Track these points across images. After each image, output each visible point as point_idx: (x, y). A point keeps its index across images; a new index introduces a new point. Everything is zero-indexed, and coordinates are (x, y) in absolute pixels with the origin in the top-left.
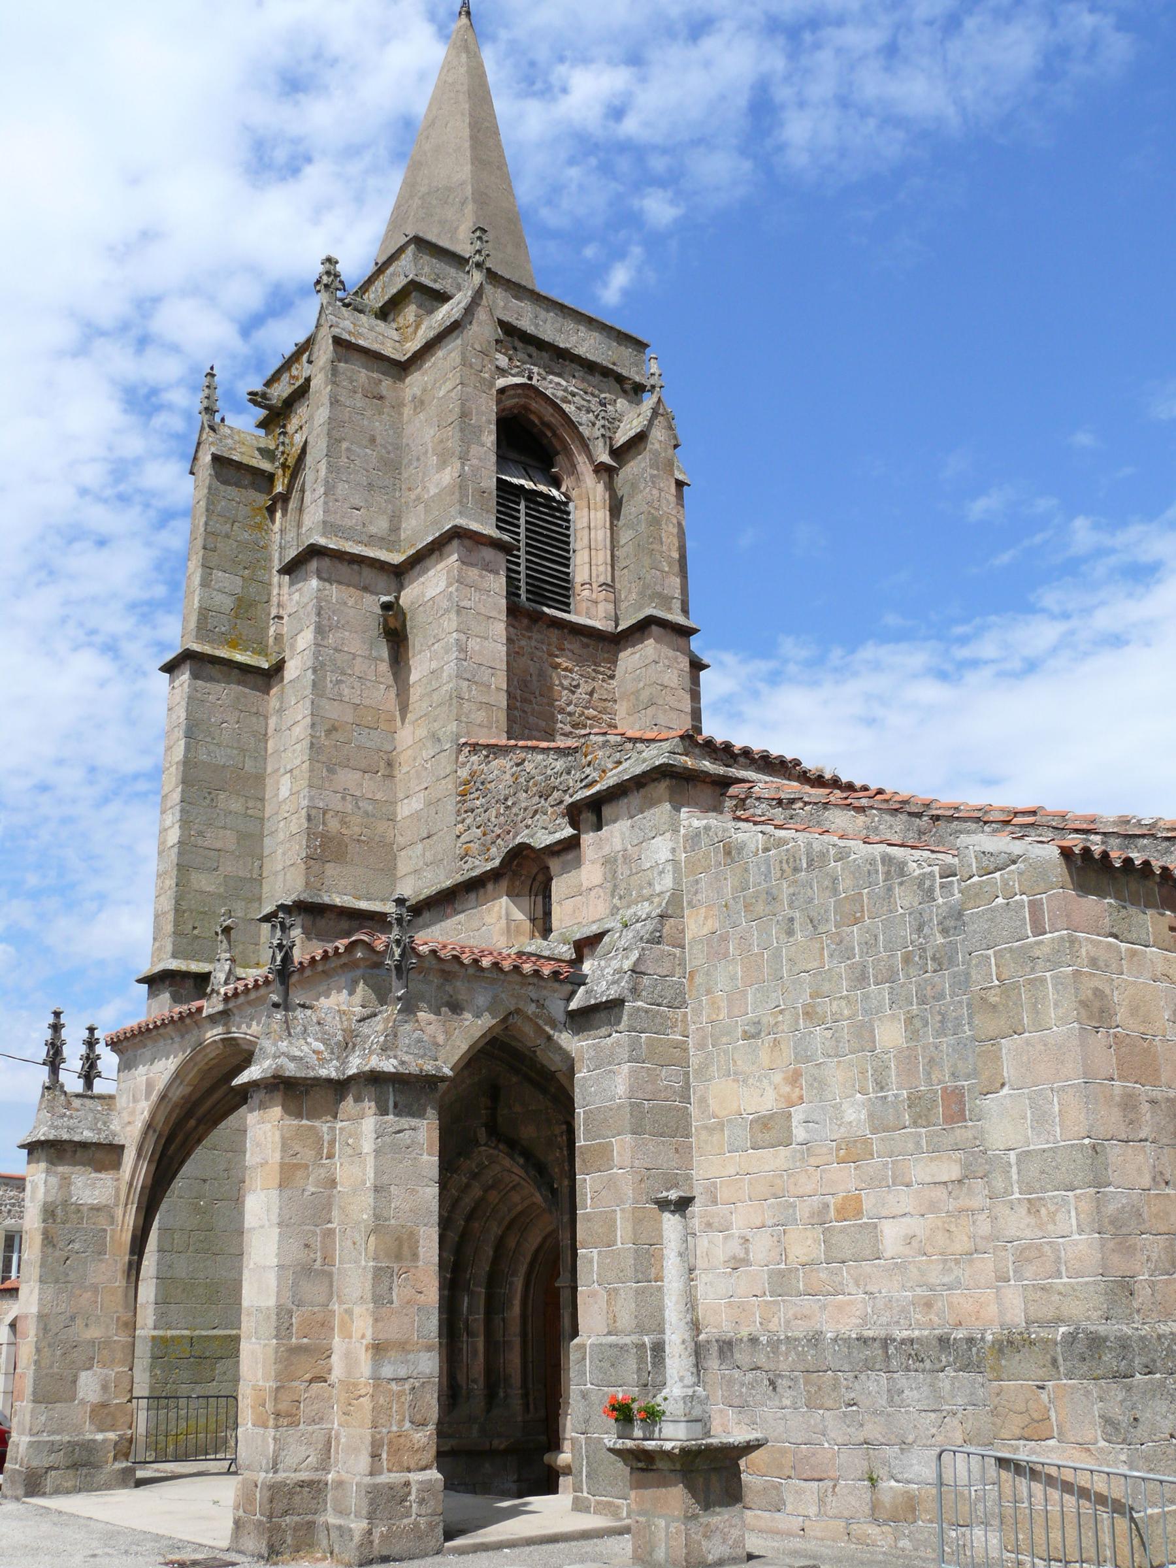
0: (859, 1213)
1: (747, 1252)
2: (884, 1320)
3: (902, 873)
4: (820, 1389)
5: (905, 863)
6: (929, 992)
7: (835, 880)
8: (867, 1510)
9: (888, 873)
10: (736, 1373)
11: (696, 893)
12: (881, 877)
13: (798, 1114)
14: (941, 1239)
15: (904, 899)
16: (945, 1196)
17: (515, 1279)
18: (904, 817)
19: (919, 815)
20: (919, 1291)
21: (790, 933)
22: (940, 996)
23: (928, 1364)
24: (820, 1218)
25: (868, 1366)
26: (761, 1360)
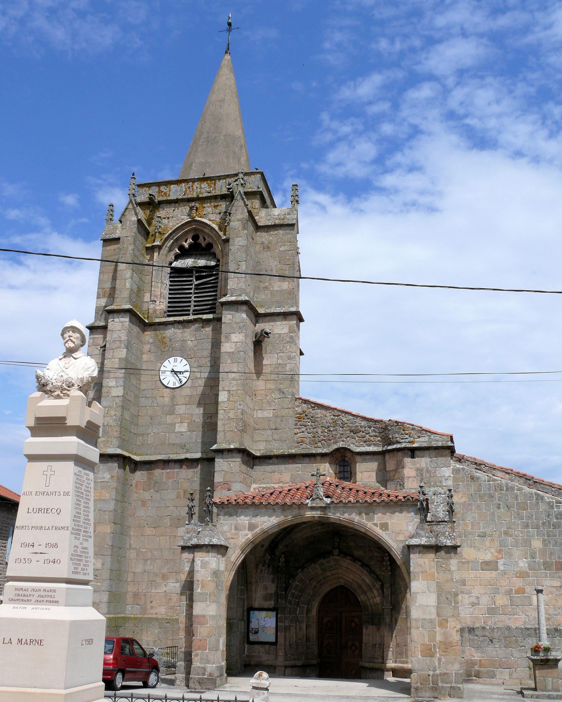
0: (524, 593)
1: (479, 602)
2: (532, 623)
3: (542, 499)
4: (510, 642)
5: (544, 497)
7: (517, 496)
8: (528, 676)
9: (537, 498)
10: (476, 637)
11: (458, 488)
13: (501, 562)
14: (554, 602)
15: (542, 507)
16: (555, 590)
17: (314, 603)
18: (524, 479)
19: (529, 480)
22: (555, 536)
24: (509, 592)
25: (529, 636)
26: (487, 634)
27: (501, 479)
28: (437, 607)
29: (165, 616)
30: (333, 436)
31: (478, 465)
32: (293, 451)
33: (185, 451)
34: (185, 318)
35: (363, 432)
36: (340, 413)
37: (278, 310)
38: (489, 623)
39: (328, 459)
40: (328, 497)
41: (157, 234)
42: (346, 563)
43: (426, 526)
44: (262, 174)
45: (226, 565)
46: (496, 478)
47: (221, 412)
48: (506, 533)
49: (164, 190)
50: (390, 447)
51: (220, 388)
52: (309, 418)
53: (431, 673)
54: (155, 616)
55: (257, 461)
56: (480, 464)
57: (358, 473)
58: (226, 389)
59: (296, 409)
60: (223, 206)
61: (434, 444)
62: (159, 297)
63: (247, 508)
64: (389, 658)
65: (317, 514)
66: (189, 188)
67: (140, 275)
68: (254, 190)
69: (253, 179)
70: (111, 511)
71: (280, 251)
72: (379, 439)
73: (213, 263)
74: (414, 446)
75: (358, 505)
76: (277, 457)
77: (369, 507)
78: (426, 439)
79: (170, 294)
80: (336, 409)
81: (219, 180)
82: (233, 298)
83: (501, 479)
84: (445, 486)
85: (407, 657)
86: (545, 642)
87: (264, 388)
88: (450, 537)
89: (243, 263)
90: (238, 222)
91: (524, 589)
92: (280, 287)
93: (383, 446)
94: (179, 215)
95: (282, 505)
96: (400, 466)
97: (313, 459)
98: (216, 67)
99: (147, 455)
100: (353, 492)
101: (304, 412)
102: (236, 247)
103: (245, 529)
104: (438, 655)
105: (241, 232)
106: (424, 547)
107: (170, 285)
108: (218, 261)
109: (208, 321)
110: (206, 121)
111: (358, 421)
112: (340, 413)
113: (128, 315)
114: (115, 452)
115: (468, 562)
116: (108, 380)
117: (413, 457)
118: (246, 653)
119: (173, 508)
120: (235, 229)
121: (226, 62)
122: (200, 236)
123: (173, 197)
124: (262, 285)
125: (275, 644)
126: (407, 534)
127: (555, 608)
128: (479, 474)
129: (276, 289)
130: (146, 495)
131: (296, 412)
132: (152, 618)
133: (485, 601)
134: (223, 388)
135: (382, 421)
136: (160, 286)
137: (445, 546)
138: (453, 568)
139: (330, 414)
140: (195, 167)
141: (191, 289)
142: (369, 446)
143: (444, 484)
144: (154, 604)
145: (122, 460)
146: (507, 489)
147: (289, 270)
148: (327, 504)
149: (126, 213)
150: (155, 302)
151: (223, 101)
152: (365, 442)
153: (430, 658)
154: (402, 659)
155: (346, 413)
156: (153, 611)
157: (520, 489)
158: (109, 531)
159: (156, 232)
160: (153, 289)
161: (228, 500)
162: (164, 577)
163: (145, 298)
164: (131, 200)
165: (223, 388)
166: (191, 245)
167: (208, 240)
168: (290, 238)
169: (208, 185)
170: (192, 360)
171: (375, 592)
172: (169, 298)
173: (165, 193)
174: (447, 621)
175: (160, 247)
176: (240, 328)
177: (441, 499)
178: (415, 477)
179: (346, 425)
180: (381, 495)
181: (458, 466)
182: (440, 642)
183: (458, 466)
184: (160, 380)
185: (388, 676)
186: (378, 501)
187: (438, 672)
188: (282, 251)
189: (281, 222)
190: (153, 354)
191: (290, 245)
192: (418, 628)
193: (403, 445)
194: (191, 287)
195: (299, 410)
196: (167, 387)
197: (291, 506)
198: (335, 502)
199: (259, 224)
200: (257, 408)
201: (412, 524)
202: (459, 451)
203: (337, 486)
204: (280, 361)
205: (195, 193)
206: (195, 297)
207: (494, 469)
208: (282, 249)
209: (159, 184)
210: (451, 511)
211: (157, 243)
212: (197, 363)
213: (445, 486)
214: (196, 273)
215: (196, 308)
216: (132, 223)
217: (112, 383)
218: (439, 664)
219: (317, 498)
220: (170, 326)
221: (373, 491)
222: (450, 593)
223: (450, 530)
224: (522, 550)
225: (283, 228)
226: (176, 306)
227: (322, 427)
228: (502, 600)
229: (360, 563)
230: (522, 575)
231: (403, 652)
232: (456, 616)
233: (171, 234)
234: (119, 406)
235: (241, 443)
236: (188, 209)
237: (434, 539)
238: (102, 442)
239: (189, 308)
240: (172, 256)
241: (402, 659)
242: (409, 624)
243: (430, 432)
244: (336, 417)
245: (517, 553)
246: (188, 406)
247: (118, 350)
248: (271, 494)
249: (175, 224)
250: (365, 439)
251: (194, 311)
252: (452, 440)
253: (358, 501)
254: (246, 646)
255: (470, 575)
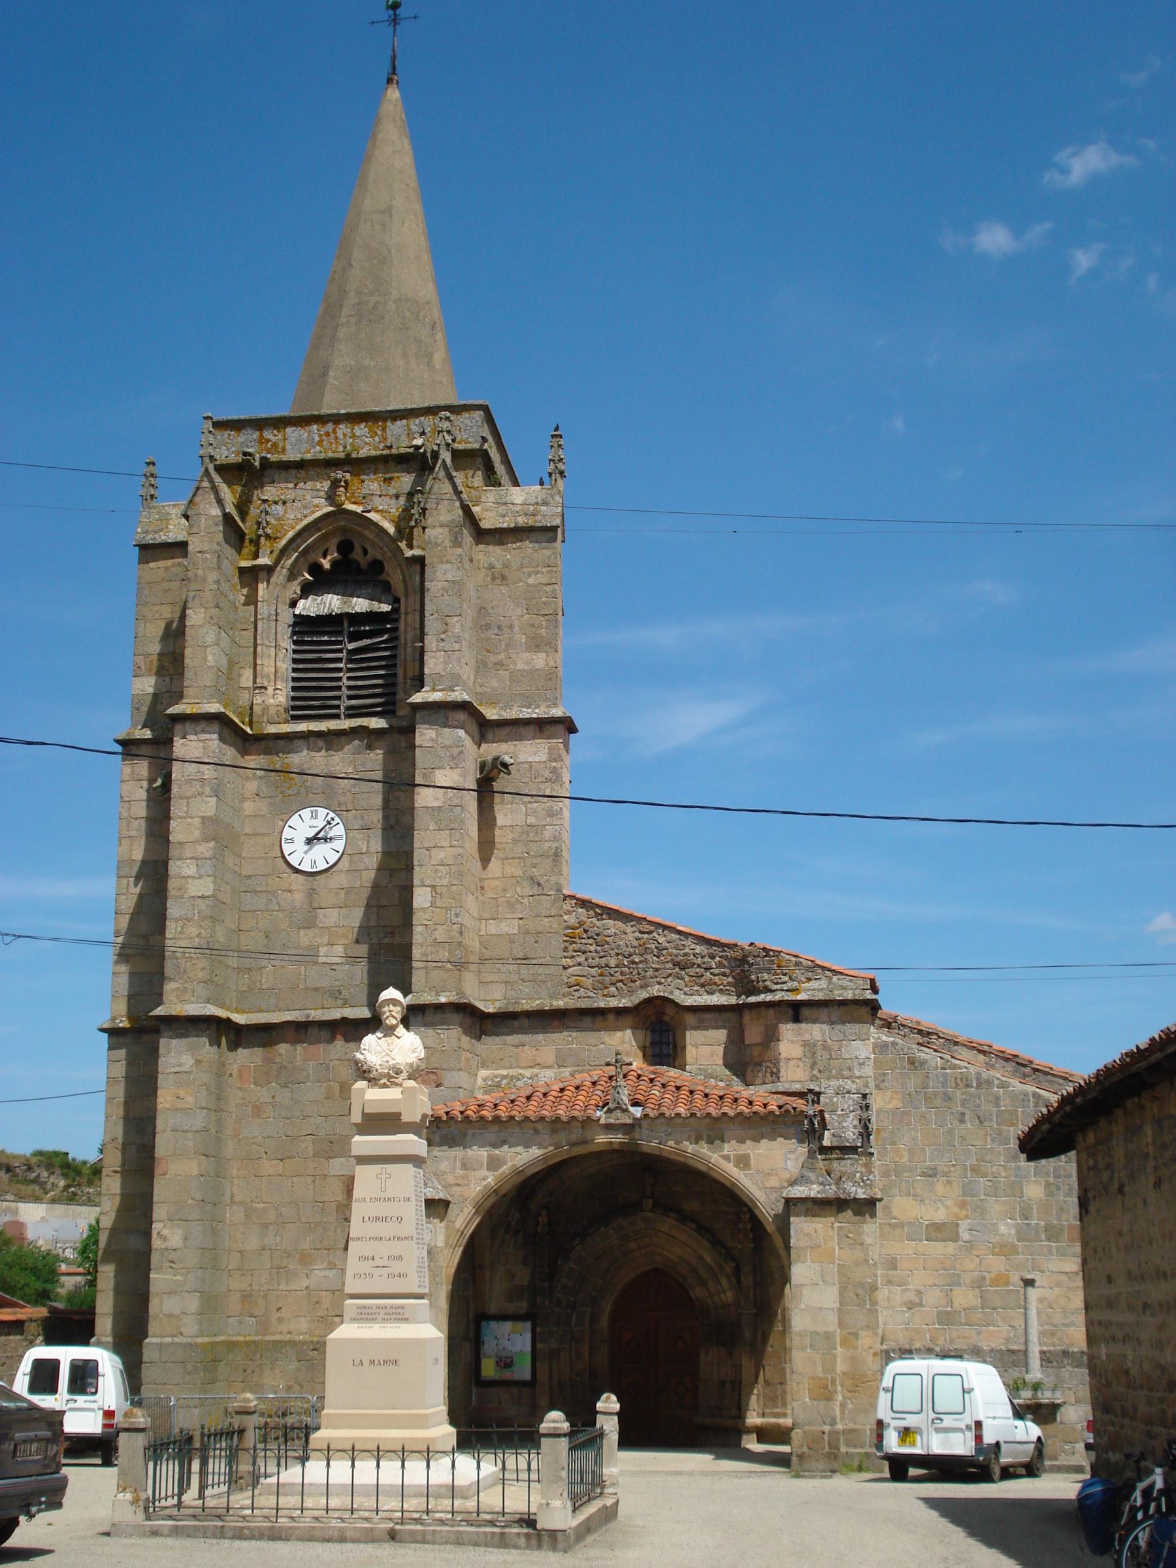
6: (1062, 1172)
7: (997, 1099)
11: (883, 1081)
12: (1032, 1104)
13: (964, 1225)
19: (1024, 1066)
20: (1046, 1327)
21: (962, 1121)
23: (1055, 1364)
24: (979, 1283)
27: (970, 1064)
28: (839, 1310)
29: (308, 1338)
30: (639, 974)
31: (925, 1035)
32: (560, 1004)
33: (340, 1002)
34: (333, 725)
35: (699, 966)
36: (652, 928)
37: (526, 713)
38: (941, 1341)
39: (629, 1020)
40: (636, 1104)
41: (263, 540)
42: (668, 1225)
43: (820, 1162)
44: (485, 409)
45: (447, 1236)
46: (957, 1062)
47: (418, 930)
48: (975, 1170)
49: (270, 437)
50: (752, 999)
51: (416, 882)
52: (592, 937)
53: (827, 1428)
54: (288, 1337)
55: (489, 1025)
56: (929, 1033)
57: (689, 1047)
58: (428, 882)
59: (566, 917)
60: (405, 481)
61: (838, 995)
62: (273, 677)
63: (485, 1127)
64: (751, 1407)
65: (618, 1138)
66: (328, 434)
67: (231, 633)
68: (469, 446)
69: (468, 422)
70: (197, 1131)
71: (528, 585)
72: (730, 979)
73: (386, 608)
74: (799, 997)
75: (692, 1120)
76: (529, 1014)
77: (714, 1129)
78: (823, 984)
79: (294, 670)
80: (645, 919)
81: (394, 420)
82: (437, 696)
83: (970, 1064)
84: (859, 1078)
85: (784, 1405)
86: (1036, 1373)
87: (499, 874)
88: (864, 1183)
89: (456, 619)
90: (441, 530)
91: (1007, 1276)
92: (528, 663)
93: (739, 996)
94: (308, 497)
95: (552, 1121)
96: (771, 1037)
97: (599, 1018)
98: (371, 121)
99: (260, 1011)
100: (684, 1092)
101: (581, 924)
102: (440, 585)
103: (481, 1168)
104: (840, 1398)
105: (450, 551)
106: (816, 1201)
107: (295, 652)
108: (396, 600)
109: (379, 732)
110: (354, 264)
111: (690, 946)
112: (652, 928)
113: (216, 726)
114: (203, 1013)
115: (902, 1225)
116: (179, 863)
117: (796, 1019)
118: (474, 1403)
119: (319, 1120)
120: (437, 545)
121: (391, 108)
122: (356, 544)
123: (292, 455)
124: (493, 659)
125: (532, 1383)
126: (786, 1176)
127: (1064, 1313)
128: (925, 1054)
129: (520, 666)
130: (263, 1094)
131: (564, 924)
132: (281, 1342)
133: (933, 1298)
134: (422, 881)
135: (736, 945)
136: (273, 654)
137: (855, 1199)
138: (868, 1240)
139: (634, 929)
140: (335, 378)
141: (340, 660)
142: (711, 993)
143: (857, 1074)
144: (283, 1313)
145: (214, 1029)
146: (979, 1085)
147: (547, 628)
148: (635, 1119)
149: (198, 499)
150: (266, 688)
151: (388, 211)
152: (702, 985)
153: (825, 1402)
154: (775, 1410)
155: (665, 927)
156: (284, 1327)
157: (1003, 1085)
158: (195, 1172)
159: (259, 536)
160: (259, 662)
161: (447, 1113)
162: (305, 1259)
163: (243, 679)
164: (207, 470)
165: (422, 881)
166: (334, 564)
167: (374, 554)
168: (549, 558)
169: (370, 431)
170: (350, 814)
171: (724, 1282)
172: (294, 679)
173: (275, 445)
174: (856, 1335)
175: (269, 570)
176: (453, 758)
177: (851, 1102)
178: (800, 1059)
179: (664, 952)
180: (736, 1100)
181: (884, 1038)
182: (844, 1373)
183: (884, 1038)
184: (283, 856)
185: (749, 1442)
186: (731, 1113)
187: (840, 1427)
188: (533, 586)
189: (531, 522)
190: (267, 802)
191: (549, 572)
192: (803, 1349)
193: (778, 996)
194: (340, 655)
195: (571, 920)
196: (297, 871)
197: (568, 1123)
198: (652, 1115)
199: (485, 525)
200: (486, 916)
201: (793, 1156)
202: (889, 1006)
203: (652, 1080)
204: (531, 820)
205: (341, 448)
206: (349, 679)
207: (956, 1043)
208: (531, 581)
209: (259, 424)
210: (866, 1132)
211: (264, 560)
212: (360, 822)
213: (859, 1078)
214: (350, 626)
215: (353, 702)
216: (211, 522)
217: (189, 869)
218: (842, 1413)
219: (616, 1108)
220: (300, 742)
221: (721, 1093)
222: (861, 1285)
223: (864, 1170)
224: (1005, 1202)
225: (533, 536)
226: (309, 699)
227: (617, 954)
228: (964, 1297)
229: (694, 1226)
230: (1005, 1249)
231: (777, 1397)
232: (872, 1327)
233: (292, 540)
234: (206, 918)
235: (460, 993)
236: (327, 485)
237: (833, 1187)
238: (173, 991)
239: (336, 702)
240: (295, 588)
241: (775, 1410)
242: (788, 1342)
243: (830, 970)
244: (646, 936)
245: (995, 1207)
246: (344, 911)
247: (199, 798)
248: (528, 1098)
249: (299, 516)
250: (702, 980)
251: (348, 708)
252: (875, 989)
253: (693, 1115)
254: (474, 1389)
255: (904, 1249)
